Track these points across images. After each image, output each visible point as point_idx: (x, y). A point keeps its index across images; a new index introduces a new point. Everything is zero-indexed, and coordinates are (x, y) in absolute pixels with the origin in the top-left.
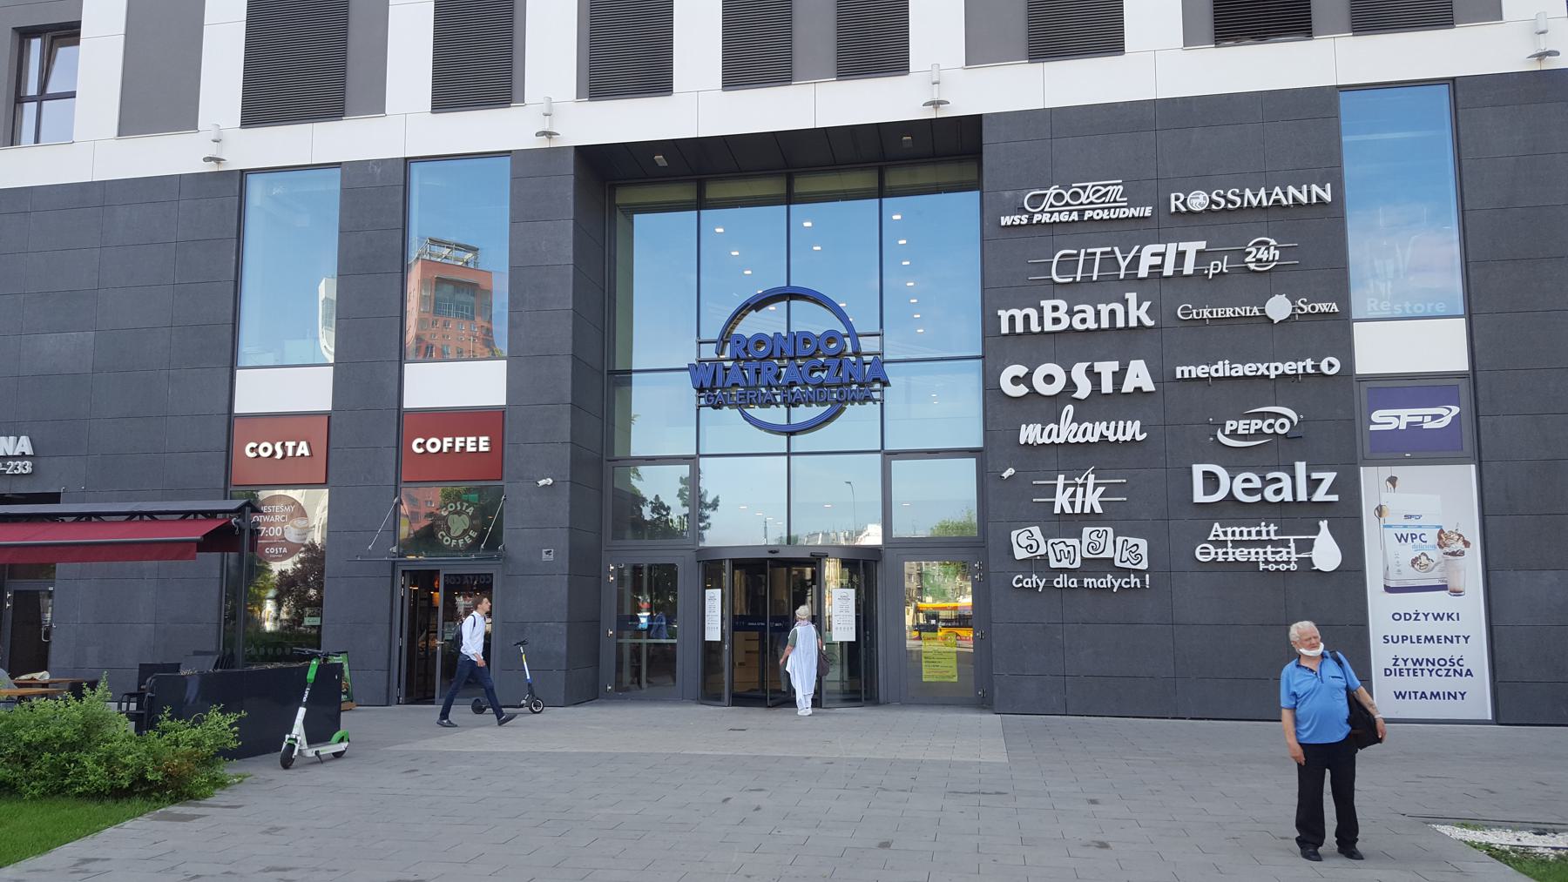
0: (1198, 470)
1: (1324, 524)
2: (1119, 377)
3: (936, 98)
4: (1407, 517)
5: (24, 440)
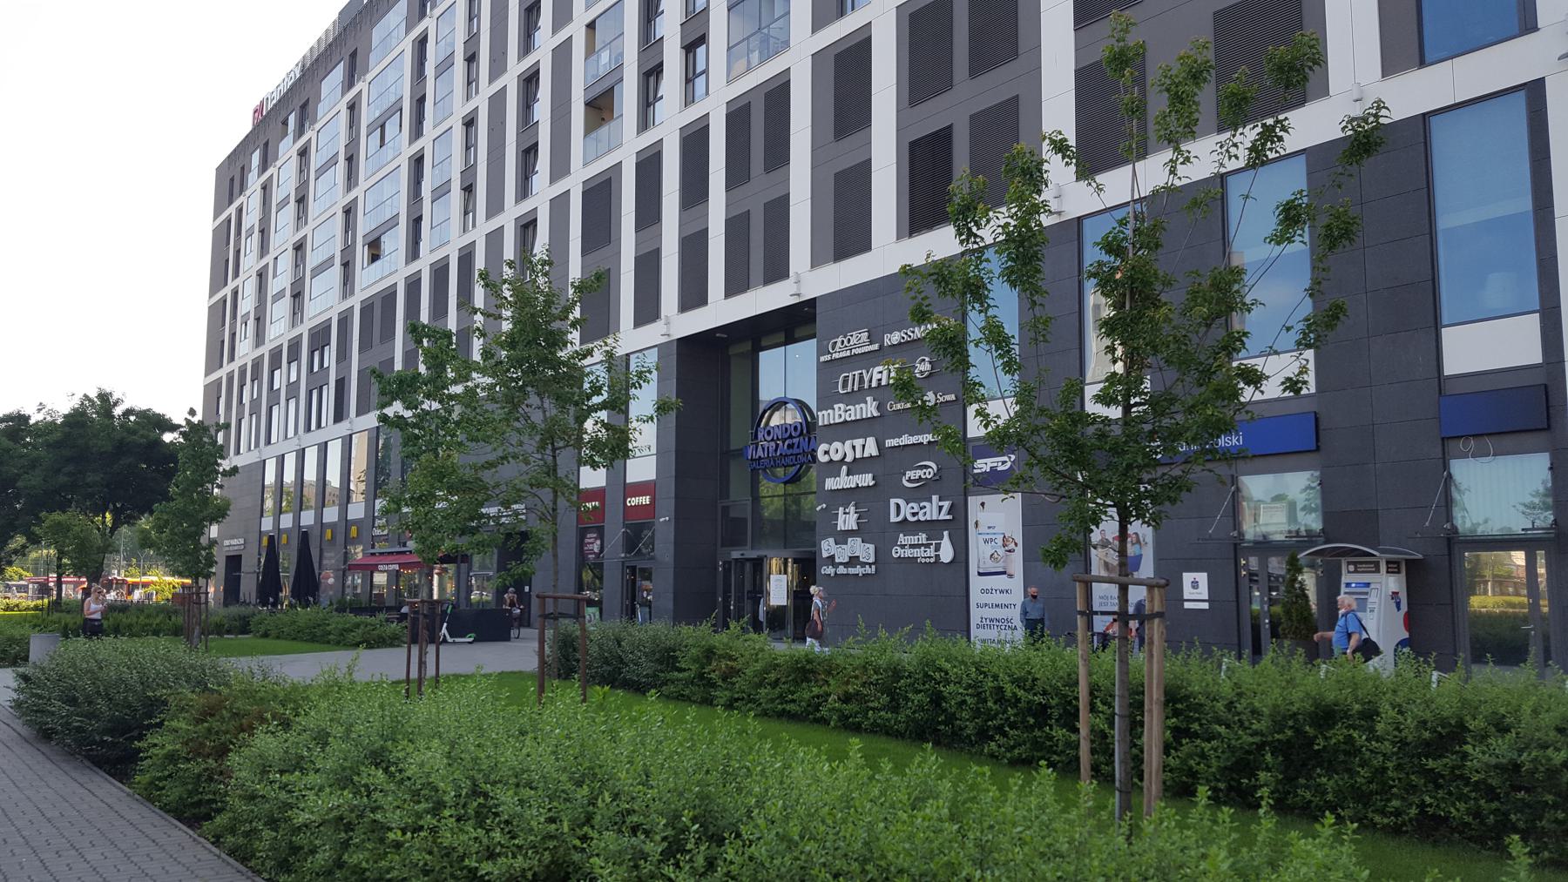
0: (893, 501)
1: (946, 533)
4: (989, 528)
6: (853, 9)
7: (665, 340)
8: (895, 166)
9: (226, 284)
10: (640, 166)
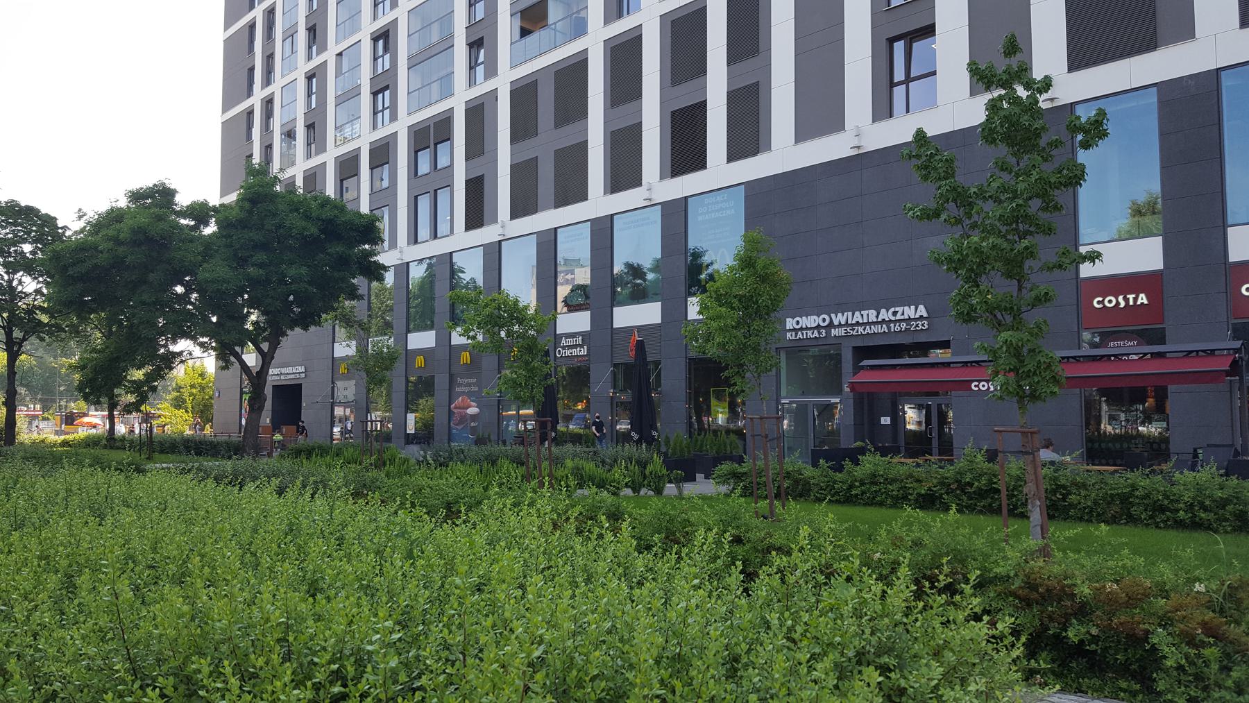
2: (1135, 299)
5: (921, 307)
6: (628, 14)
7: (399, 262)
8: (658, 129)
9: (250, 93)
10: (469, 112)
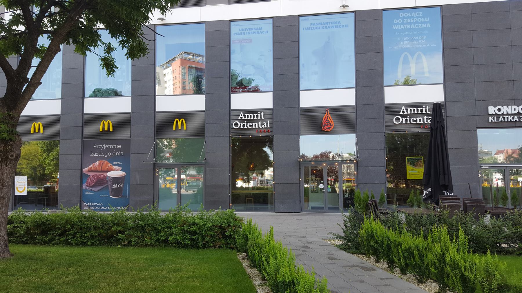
3: (344, 4)
